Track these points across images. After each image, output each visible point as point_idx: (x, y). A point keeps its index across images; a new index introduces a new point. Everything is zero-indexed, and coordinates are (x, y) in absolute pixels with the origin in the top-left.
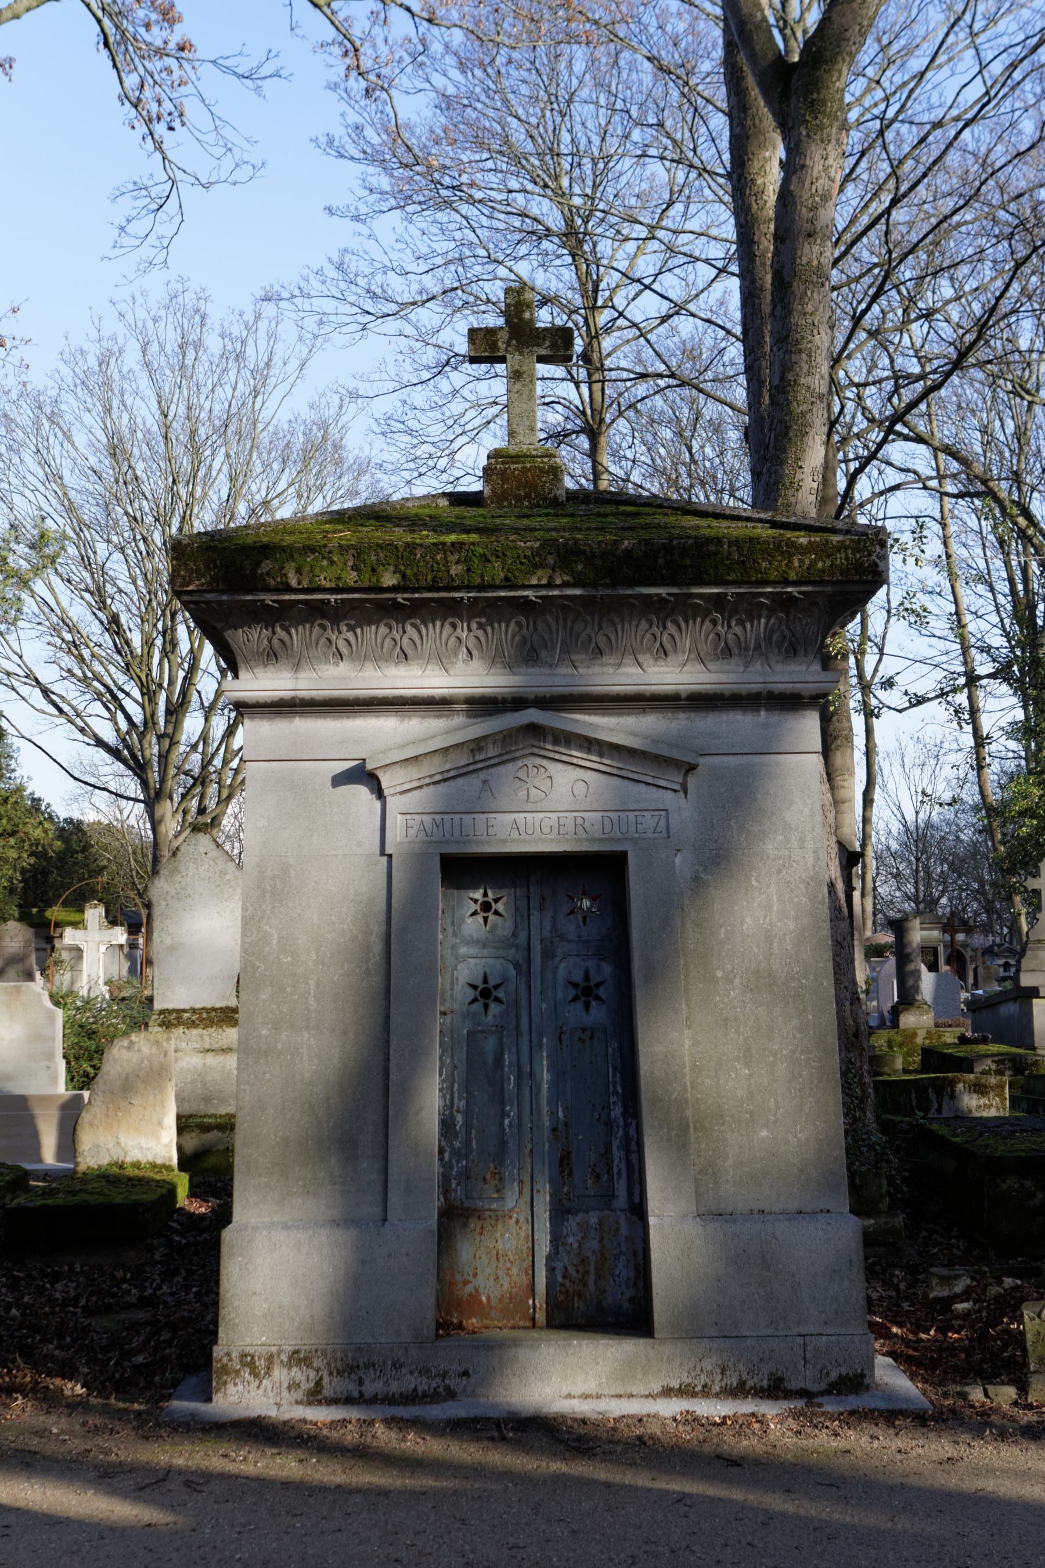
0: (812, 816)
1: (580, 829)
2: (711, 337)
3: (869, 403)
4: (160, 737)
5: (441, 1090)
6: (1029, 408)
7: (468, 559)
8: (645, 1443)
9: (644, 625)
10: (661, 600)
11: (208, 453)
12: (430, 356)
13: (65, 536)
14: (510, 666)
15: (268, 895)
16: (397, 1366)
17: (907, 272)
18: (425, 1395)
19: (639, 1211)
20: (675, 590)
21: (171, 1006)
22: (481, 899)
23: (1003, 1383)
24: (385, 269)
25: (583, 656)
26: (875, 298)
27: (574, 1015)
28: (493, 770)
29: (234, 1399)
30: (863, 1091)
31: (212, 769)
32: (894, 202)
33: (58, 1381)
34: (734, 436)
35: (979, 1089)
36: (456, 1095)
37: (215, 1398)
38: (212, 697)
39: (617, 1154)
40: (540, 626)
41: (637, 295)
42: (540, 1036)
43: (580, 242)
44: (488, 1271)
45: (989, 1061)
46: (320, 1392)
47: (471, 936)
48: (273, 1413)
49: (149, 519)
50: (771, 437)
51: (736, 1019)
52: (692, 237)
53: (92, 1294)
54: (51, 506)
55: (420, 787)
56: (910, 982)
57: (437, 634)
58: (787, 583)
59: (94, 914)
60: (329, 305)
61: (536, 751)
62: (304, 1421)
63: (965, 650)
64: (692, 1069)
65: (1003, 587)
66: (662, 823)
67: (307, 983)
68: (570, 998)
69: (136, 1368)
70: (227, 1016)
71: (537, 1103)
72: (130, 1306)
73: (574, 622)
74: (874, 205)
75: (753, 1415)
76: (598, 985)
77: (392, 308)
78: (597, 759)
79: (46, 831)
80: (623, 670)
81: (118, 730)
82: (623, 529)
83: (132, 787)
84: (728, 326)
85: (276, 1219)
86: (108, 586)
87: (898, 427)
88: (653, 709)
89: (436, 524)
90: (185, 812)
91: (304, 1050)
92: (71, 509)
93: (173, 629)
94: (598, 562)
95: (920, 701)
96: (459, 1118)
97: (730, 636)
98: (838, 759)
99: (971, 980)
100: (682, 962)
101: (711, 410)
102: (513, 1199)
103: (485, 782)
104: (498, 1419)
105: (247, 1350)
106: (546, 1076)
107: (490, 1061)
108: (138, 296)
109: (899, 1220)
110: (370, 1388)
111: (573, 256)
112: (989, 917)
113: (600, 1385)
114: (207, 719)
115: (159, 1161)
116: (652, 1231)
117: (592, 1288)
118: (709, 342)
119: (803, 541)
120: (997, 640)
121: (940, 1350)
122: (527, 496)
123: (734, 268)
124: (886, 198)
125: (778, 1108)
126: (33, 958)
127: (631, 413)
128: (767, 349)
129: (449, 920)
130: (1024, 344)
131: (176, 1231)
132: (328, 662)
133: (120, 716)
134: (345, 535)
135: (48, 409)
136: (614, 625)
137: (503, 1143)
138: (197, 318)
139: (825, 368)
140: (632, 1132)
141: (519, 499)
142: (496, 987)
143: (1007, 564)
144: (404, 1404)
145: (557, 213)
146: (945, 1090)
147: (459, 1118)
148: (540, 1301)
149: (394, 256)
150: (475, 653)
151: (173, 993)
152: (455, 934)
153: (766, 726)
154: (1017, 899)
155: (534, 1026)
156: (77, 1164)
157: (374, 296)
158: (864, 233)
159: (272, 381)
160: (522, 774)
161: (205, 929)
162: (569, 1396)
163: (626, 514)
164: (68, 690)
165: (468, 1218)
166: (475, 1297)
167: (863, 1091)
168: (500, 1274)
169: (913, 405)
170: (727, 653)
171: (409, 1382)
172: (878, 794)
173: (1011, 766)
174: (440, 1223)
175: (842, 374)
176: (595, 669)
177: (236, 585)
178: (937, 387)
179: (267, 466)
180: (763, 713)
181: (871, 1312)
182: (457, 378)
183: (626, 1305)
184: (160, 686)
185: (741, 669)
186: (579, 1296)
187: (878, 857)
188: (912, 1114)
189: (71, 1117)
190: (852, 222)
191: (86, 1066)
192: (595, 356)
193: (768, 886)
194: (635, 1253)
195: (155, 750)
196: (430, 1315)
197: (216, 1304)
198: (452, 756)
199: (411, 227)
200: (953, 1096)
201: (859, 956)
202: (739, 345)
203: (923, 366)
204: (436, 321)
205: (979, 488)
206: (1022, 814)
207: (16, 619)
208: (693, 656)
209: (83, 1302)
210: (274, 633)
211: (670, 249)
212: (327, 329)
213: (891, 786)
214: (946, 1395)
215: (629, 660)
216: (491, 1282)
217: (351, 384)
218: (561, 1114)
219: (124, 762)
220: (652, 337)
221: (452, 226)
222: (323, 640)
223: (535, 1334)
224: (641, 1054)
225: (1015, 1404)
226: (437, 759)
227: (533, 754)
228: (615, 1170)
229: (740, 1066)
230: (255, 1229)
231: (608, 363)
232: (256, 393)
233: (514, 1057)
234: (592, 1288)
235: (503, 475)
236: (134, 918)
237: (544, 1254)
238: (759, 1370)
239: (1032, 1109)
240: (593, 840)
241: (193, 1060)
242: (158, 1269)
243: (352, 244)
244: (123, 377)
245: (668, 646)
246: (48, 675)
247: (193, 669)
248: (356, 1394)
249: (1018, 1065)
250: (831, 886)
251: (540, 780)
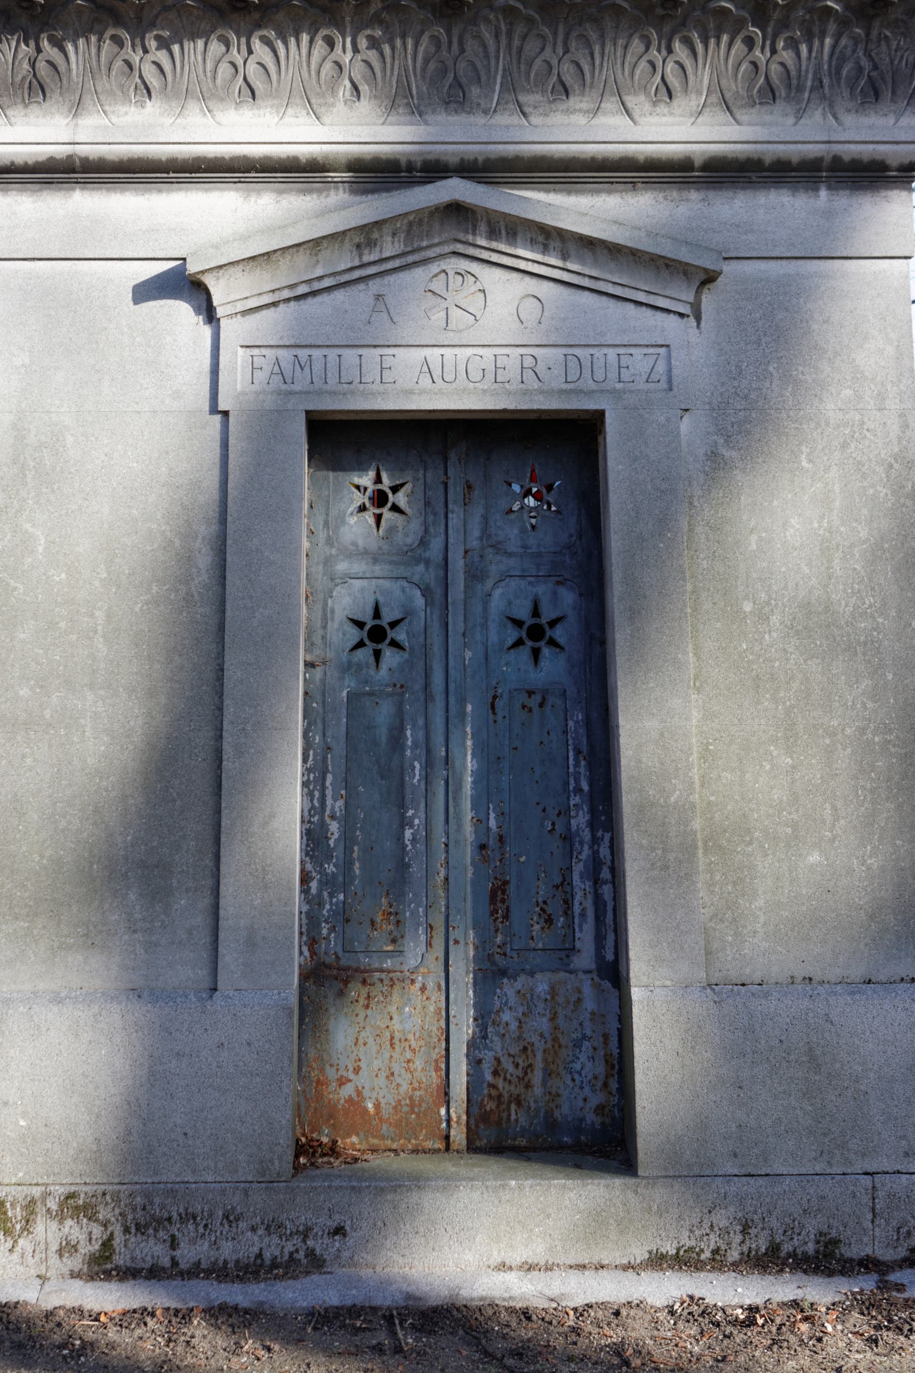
1: (529, 375)
5: (305, 784)
8: (627, 1363)
9: (637, 45)
15: (30, 476)
16: (230, 1218)
18: (274, 1265)
19: (614, 974)
22: (371, 487)
25: (538, 97)
27: (516, 668)
28: (391, 279)
36: (329, 793)
39: (580, 886)
42: (462, 702)
44: (377, 1064)
46: (109, 1258)
47: (355, 544)
51: (773, 678)
55: (274, 304)
61: (460, 248)
62: (79, 1312)
64: (703, 757)
66: (661, 367)
67: (92, 615)
68: (510, 642)
71: (457, 805)
73: (524, 38)
75: (795, 1304)
76: (553, 624)
78: (559, 263)
80: (601, 120)
85: (41, 986)
88: (648, 183)
96: (334, 827)
97: (774, 68)
100: (689, 587)
102: (416, 953)
103: (378, 297)
104: (389, 1309)
106: (470, 763)
107: (384, 740)
110: (188, 1254)
113: (551, 1249)
116: (636, 1010)
117: (538, 1091)
125: (836, 819)
129: (320, 519)
132: (127, 100)
136: (589, 45)
137: (402, 867)
140: (604, 851)
142: (393, 624)
144: (241, 1279)
147: (334, 827)
148: (458, 1108)
150: (364, 88)
152: (329, 542)
155: (452, 686)
160: (438, 285)
162: (503, 1267)
165: (346, 983)
166: (356, 1103)
168: (396, 1068)
170: (769, 94)
174: (302, 991)
176: (557, 118)
180: (823, 193)
183: (590, 1117)
185: (791, 120)
186: (519, 1104)
193: (827, 469)
194: (606, 1037)
208: (714, 99)
210: (39, 50)
215: (611, 103)
216: (382, 1081)
218: (493, 823)
222: (118, 64)
223: (448, 1166)
224: (622, 731)
226: (302, 259)
227: (455, 253)
228: (577, 909)
233: (421, 734)
234: (538, 1091)
237: (465, 1038)
238: (802, 1227)
240: (550, 393)
248: (166, 1262)
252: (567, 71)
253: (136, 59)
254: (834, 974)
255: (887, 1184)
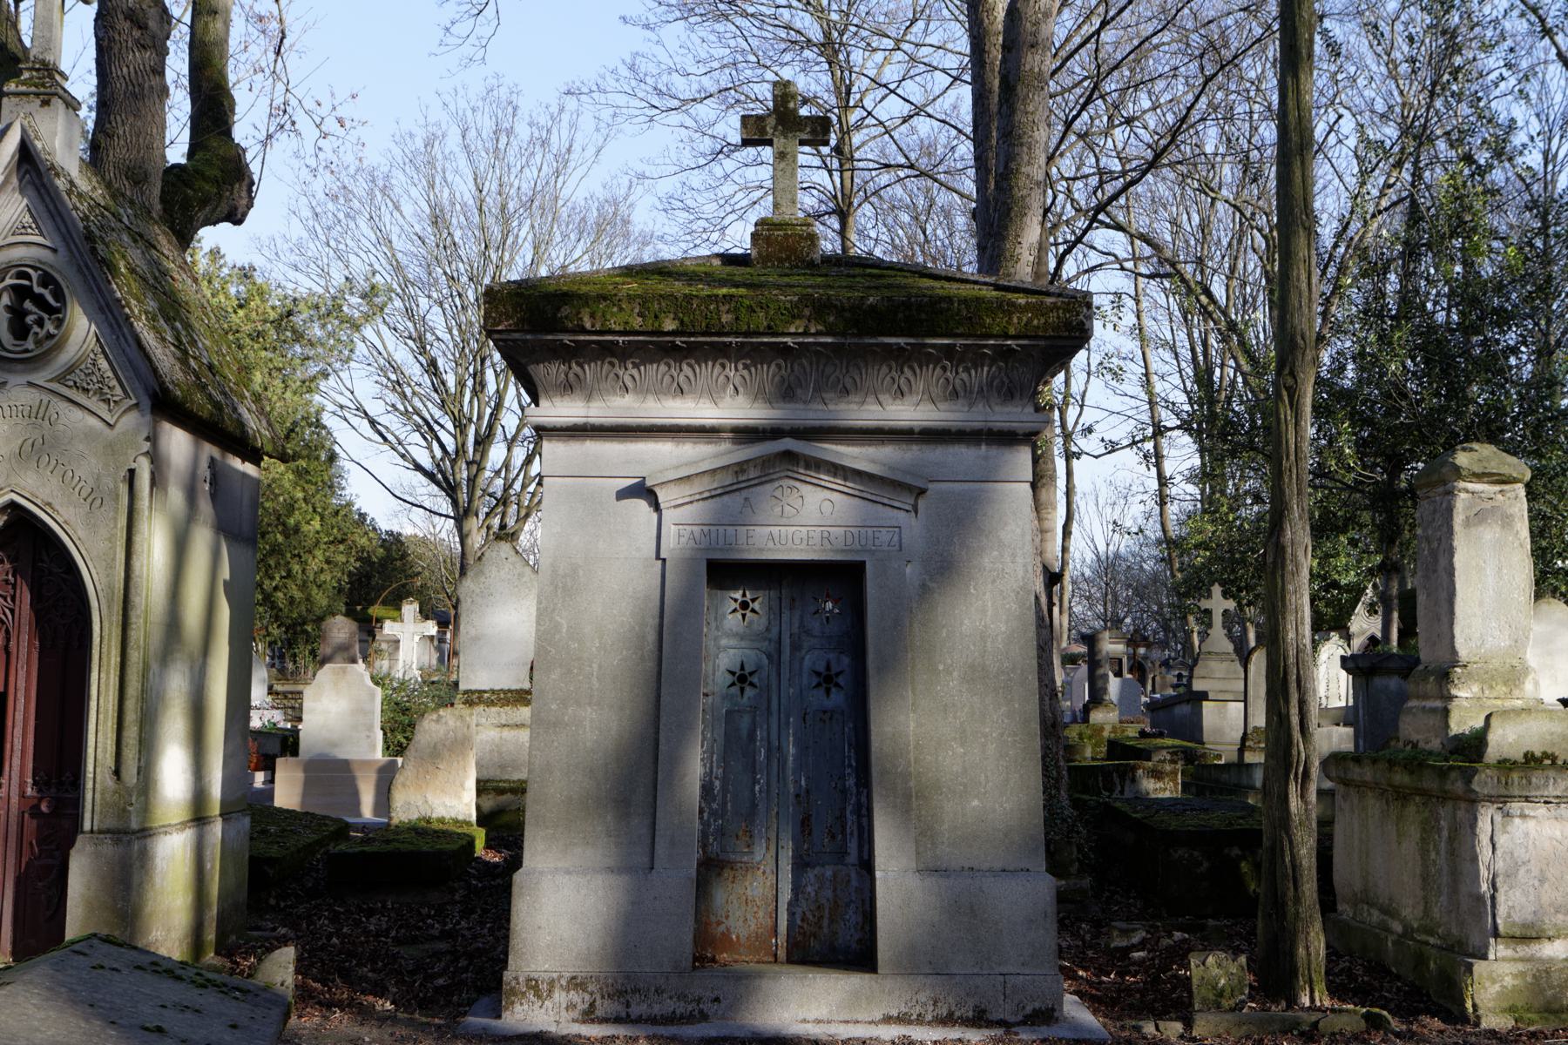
0: (1023, 535)
2: (945, 136)
3: (1076, 196)
4: (469, 464)
6: (1212, 204)
7: (736, 310)
9: (885, 369)
10: (900, 348)
11: (515, 224)
12: (707, 145)
13: (391, 290)
14: (770, 402)
16: (659, 991)
17: (1110, 85)
18: (682, 1017)
19: (867, 866)
20: (912, 341)
21: (473, 687)
23: (1171, 1020)
24: (670, 71)
26: (1084, 107)
27: (817, 698)
29: (518, 1017)
30: (1059, 773)
31: (512, 492)
32: (1104, 24)
33: (371, 999)
34: (961, 221)
35: (1157, 774)
37: (504, 1015)
38: (514, 431)
39: (851, 818)
40: (796, 367)
41: (883, 98)
43: (836, 52)
45: (1164, 752)
48: (553, 1029)
49: (464, 279)
50: (995, 218)
52: (932, 50)
53: (401, 927)
54: (382, 266)
56: (1100, 684)
57: (709, 372)
58: (1007, 336)
59: (410, 609)
60: (621, 100)
62: (580, 1036)
63: (1152, 404)
65: (1185, 353)
66: (896, 538)
69: (437, 990)
70: (520, 697)
72: (433, 938)
74: (1085, 28)
76: (838, 674)
77: (676, 103)
79: (370, 540)
80: (866, 407)
81: (433, 457)
82: (869, 288)
83: (445, 505)
84: (960, 126)
86: (428, 335)
87: (1101, 217)
88: (891, 441)
89: (708, 278)
90: (488, 528)
91: (587, 723)
92: (398, 268)
93: (483, 373)
94: (847, 315)
95: (1112, 447)
96: (717, 783)
98: (1043, 495)
99: (1149, 688)
101: (943, 198)
102: (760, 853)
103: (746, 499)
105: (533, 975)
106: (792, 750)
108: (460, 89)
109: (1086, 882)
110: (635, 1010)
111: (830, 63)
112: (1166, 635)
114: (509, 450)
115: (460, 818)
118: (943, 140)
119: (1022, 301)
120: (1181, 398)
121: (1119, 991)
122: (788, 258)
123: (968, 78)
124: (1097, 22)
126: (357, 647)
127: (874, 199)
128: (994, 142)
130: (1209, 149)
131: (473, 876)
133: (435, 445)
134: (633, 286)
135: (380, 183)
137: (754, 806)
138: (510, 109)
139: (1043, 160)
140: (863, 799)
141: (781, 261)
142: (751, 674)
143: (1190, 335)
145: (816, 26)
146: (1128, 774)
147: (717, 783)
149: (678, 59)
150: (741, 390)
151: (476, 676)
152: (717, 628)
153: (986, 458)
154: (1191, 618)
156: (390, 818)
157: (660, 93)
158: (1076, 50)
159: (572, 164)
160: (778, 493)
161: (505, 624)
162: (804, 1021)
163: (870, 275)
164: (392, 422)
166: (726, 935)
167: (1059, 773)
169: (1115, 197)
170: (955, 395)
171: (669, 1006)
172: (1075, 528)
173: (1189, 507)
175: (1054, 170)
176: (842, 406)
177: (539, 327)
178: (1133, 182)
179: (565, 236)
181: (1061, 958)
182: (729, 165)
183: (854, 946)
184: (470, 420)
187: (1074, 582)
188: (1099, 794)
189: (386, 779)
190: (1068, 40)
191: (400, 737)
192: (846, 149)
195: (465, 475)
196: (688, 949)
197: (507, 938)
198: (718, 476)
199: (693, 36)
200: (1134, 780)
201: (1057, 662)
202: (969, 144)
203: (1123, 165)
204: (712, 115)
205: (1167, 269)
206: (1197, 547)
207: (349, 359)
209: (393, 933)
211: (912, 59)
212: (619, 120)
213: (1086, 521)
214: (1123, 1028)
215: (871, 399)
217: (640, 168)
219: (438, 484)
220: (896, 134)
221: (728, 35)
223: (776, 968)
225: (1182, 1037)
226: (706, 479)
229: (959, 740)
230: (541, 873)
231: (857, 155)
232: (557, 173)
235: (768, 239)
236: (445, 617)
239: (1200, 792)
240: (837, 551)
241: (491, 733)
242: (458, 907)
243: (643, 48)
244: (445, 158)
245: (905, 388)
246: (375, 409)
247: (498, 406)
248: (623, 1015)
249: (1189, 757)
250: (1037, 598)
251: (793, 499)
252: (848, 381)
253: (621, 373)
254: (986, 866)
255: (1011, 980)
